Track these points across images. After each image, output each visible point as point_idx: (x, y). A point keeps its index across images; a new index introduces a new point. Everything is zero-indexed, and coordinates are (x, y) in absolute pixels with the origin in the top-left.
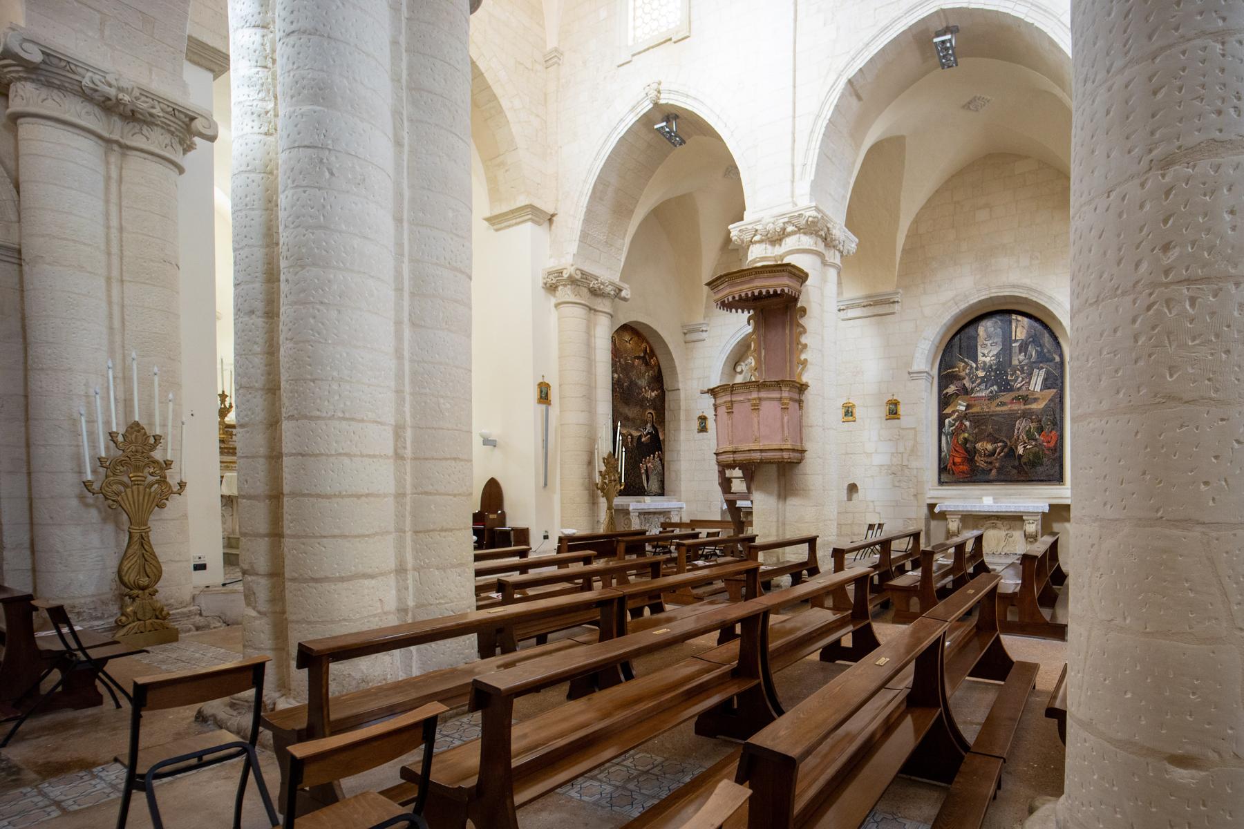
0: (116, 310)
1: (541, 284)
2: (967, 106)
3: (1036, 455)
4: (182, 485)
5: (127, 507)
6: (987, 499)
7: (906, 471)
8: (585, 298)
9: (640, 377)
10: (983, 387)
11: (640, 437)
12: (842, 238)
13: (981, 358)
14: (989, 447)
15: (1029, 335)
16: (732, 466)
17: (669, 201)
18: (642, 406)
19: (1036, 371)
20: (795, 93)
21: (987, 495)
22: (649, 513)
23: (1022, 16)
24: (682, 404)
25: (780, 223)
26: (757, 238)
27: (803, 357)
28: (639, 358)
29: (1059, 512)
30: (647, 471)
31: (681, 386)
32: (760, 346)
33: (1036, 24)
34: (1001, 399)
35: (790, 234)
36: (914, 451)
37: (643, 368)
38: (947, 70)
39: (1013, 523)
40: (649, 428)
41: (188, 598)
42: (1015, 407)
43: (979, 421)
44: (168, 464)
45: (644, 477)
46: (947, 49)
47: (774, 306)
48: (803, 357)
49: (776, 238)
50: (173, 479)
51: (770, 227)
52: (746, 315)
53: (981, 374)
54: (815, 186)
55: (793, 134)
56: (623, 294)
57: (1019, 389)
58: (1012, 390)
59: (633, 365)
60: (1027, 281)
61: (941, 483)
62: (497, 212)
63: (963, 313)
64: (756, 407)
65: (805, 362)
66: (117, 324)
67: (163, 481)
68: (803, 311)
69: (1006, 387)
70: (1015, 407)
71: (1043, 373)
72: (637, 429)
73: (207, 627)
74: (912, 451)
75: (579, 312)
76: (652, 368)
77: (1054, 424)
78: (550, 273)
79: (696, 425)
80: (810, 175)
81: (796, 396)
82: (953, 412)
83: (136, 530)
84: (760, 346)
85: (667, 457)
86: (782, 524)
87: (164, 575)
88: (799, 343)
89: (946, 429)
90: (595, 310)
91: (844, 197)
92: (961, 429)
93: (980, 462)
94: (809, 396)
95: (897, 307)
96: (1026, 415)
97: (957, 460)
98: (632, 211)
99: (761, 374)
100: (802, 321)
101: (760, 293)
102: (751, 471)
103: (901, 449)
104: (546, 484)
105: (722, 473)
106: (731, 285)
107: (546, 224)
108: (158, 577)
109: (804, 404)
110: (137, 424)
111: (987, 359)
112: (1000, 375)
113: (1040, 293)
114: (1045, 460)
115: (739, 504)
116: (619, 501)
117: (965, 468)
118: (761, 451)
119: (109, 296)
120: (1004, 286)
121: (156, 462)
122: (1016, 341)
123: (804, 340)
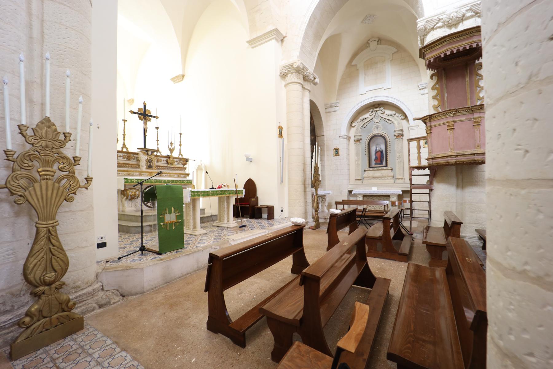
0: (36, 24)
1: (279, 74)
4: (88, 180)
5: (34, 201)
31: (325, 134)
39: (380, 198)
41: (92, 277)
44: (77, 160)
48: (481, 95)
50: (80, 172)
62: (254, 36)
66: (36, 33)
67: (71, 176)
73: (108, 303)
75: (299, 87)
79: (333, 152)
83: (43, 225)
87: (71, 261)
88: (478, 86)
107: (280, 43)
108: (64, 270)
110: (48, 120)
119: (29, 8)
121: (65, 158)
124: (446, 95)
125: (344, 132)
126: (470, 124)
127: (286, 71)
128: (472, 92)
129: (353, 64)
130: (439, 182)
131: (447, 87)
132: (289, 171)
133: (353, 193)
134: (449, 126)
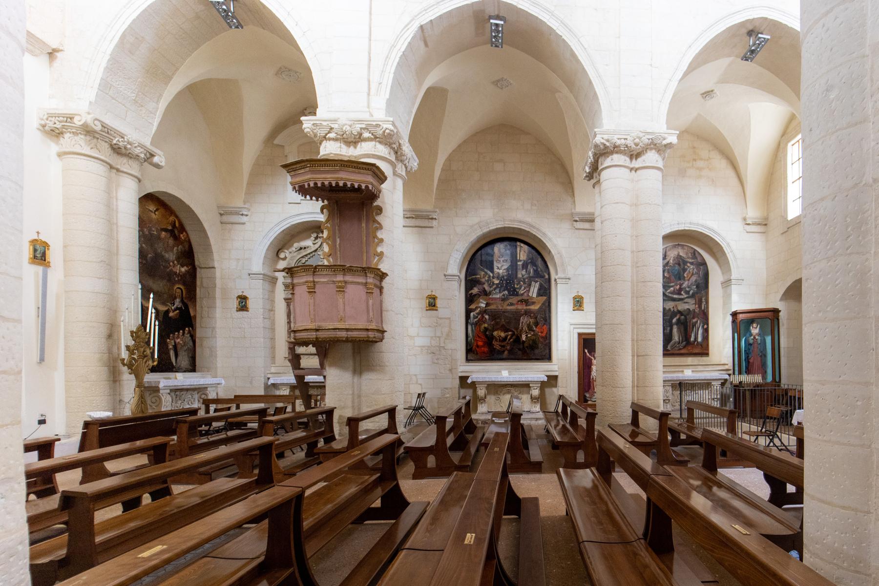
2: (496, 83)
3: (534, 341)
6: (504, 372)
7: (443, 351)
8: (106, 153)
9: (171, 254)
10: (497, 291)
11: (167, 312)
12: (409, 156)
13: (496, 270)
14: (503, 335)
15: (529, 258)
16: (305, 343)
17: (209, 80)
18: (169, 280)
19: (533, 283)
20: (371, 19)
21: (505, 369)
22: (182, 390)
23: (555, 28)
24: (218, 282)
25: (358, 127)
26: (332, 135)
27: (379, 250)
28: (166, 230)
29: (553, 380)
30: (175, 347)
31: (216, 265)
32: (334, 233)
33: (564, 37)
34: (510, 301)
35: (366, 140)
36: (449, 335)
37: (171, 241)
38: (494, 48)
39: (522, 389)
40: (178, 303)
42: (520, 307)
43: (495, 315)
45: (172, 353)
46: (498, 32)
47: (350, 199)
48: (379, 250)
49: (354, 140)
51: (347, 128)
52: (320, 203)
53: (496, 281)
54: (389, 103)
55: (369, 54)
56: (156, 159)
57: (522, 295)
58: (517, 295)
59: (159, 238)
60: (529, 219)
61: (468, 360)
63: (484, 236)
64: (341, 289)
65: (381, 255)
68: (380, 210)
69: (514, 292)
70: (520, 307)
71: (537, 285)
72: (164, 304)
74: (448, 335)
76: (182, 243)
77: (546, 320)
78: (50, 116)
80: (385, 94)
81: (378, 283)
82: (477, 308)
84: (334, 233)
85: (199, 333)
86: (358, 396)
88: (375, 237)
89: (472, 320)
90: (118, 170)
91: (408, 122)
92: (482, 321)
93: (497, 345)
94: (386, 283)
95: (434, 223)
96: (527, 313)
97: (480, 343)
98: (170, 78)
99: (335, 259)
100: (379, 218)
101: (345, 185)
102: (326, 348)
103: (439, 334)
104: (42, 359)
105: (292, 350)
106: (312, 172)
107: (46, 58)
109: (385, 290)
111: (501, 271)
112: (509, 284)
113: (538, 229)
114: (540, 345)
115: (309, 378)
116: (150, 378)
117: (486, 349)
118: (347, 330)
120: (514, 221)
122: (520, 261)
123: (380, 235)
124: (338, 241)
125: (258, 265)
126: (332, 288)
127: (58, 125)
128: (368, 244)
129: (276, 142)
130: (331, 365)
131: (339, 230)
132: (66, 337)
133: (469, 381)
134: (309, 288)
